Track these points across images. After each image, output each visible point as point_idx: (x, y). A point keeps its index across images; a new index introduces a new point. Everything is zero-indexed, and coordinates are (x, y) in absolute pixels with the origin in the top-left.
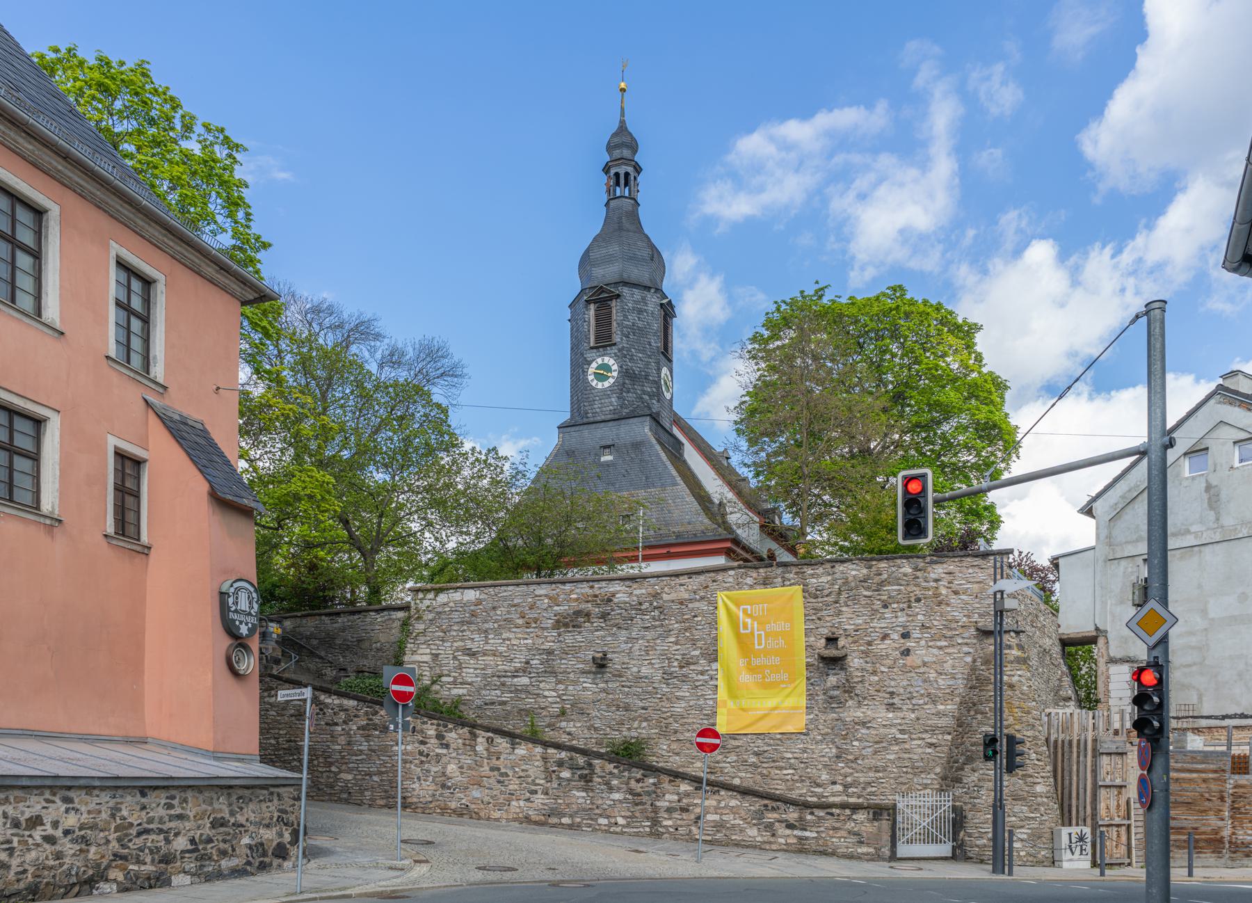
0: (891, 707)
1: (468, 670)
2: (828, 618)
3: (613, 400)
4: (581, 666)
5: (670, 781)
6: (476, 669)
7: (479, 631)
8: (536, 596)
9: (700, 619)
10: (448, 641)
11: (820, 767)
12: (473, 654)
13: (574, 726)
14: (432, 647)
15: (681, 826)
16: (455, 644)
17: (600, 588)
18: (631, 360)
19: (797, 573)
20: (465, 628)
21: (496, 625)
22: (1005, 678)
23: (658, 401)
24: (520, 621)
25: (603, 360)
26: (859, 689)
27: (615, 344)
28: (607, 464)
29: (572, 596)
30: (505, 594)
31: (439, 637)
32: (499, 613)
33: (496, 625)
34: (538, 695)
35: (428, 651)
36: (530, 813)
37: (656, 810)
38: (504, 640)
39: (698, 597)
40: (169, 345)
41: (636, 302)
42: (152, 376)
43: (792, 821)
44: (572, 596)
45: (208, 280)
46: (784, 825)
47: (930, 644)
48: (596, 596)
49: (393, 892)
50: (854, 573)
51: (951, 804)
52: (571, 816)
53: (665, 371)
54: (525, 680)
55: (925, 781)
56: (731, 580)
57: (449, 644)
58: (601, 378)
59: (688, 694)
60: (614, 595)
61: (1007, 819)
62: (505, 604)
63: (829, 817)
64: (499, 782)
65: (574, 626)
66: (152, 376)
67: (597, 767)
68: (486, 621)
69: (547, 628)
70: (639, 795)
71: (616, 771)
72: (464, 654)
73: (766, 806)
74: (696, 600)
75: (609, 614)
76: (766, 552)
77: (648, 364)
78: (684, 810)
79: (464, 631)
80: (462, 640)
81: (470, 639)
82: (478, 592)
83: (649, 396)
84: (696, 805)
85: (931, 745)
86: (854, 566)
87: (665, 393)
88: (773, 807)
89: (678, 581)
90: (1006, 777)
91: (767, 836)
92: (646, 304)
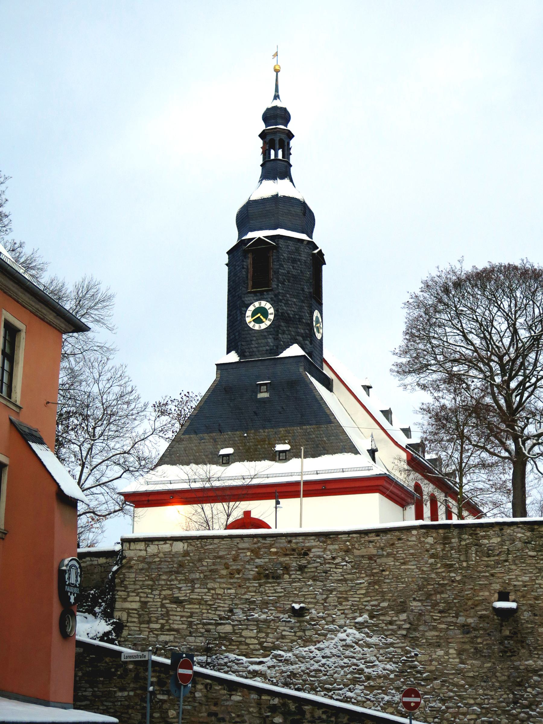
1: (175, 618)
2: (499, 575)
3: (269, 340)
6: (182, 616)
7: (186, 580)
9: (387, 573)
10: (156, 589)
11: (500, 712)
12: (177, 601)
14: (142, 595)
16: (164, 593)
17: (297, 543)
18: (286, 304)
19: (471, 535)
20: (173, 577)
21: (202, 575)
23: (311, 343)
24: (224, 572)
25: (260, 304)
26: (530, 640)
27: (271, 290)
28: (263, 400)
29: (272, 550)
30: (211, 547)
31: (148, 585)
32: (205, 564)
33: (202, 575)
34: (240, 642)
35: (137, 599)
38: (209, 589)
39: (385, 553)
40: (25, 375)
41: (290, 253)
42: (13, 400)
44: (272, 550)
45: (47, 323)
48: (294, 550)
50: (519, 535)
53: (316, 313)
54: (228, 628)
57: (157, 592)
60: (309, 550)
62: (211, 556)
65: (273, 578)
66: (13, 400)
68: (191, 572)
69: (249, 579)
71: (324, 717)
72: (172, 602)
74: (383, 556)
75: (305, 567)
77: (301, 308)
79: (172, 580)
80: (170, 589)
82: (186, 545)
83: (303, 337)
86: (519, 530)
87: (317, 334)
89: (367, 538)
92: (300, 254)
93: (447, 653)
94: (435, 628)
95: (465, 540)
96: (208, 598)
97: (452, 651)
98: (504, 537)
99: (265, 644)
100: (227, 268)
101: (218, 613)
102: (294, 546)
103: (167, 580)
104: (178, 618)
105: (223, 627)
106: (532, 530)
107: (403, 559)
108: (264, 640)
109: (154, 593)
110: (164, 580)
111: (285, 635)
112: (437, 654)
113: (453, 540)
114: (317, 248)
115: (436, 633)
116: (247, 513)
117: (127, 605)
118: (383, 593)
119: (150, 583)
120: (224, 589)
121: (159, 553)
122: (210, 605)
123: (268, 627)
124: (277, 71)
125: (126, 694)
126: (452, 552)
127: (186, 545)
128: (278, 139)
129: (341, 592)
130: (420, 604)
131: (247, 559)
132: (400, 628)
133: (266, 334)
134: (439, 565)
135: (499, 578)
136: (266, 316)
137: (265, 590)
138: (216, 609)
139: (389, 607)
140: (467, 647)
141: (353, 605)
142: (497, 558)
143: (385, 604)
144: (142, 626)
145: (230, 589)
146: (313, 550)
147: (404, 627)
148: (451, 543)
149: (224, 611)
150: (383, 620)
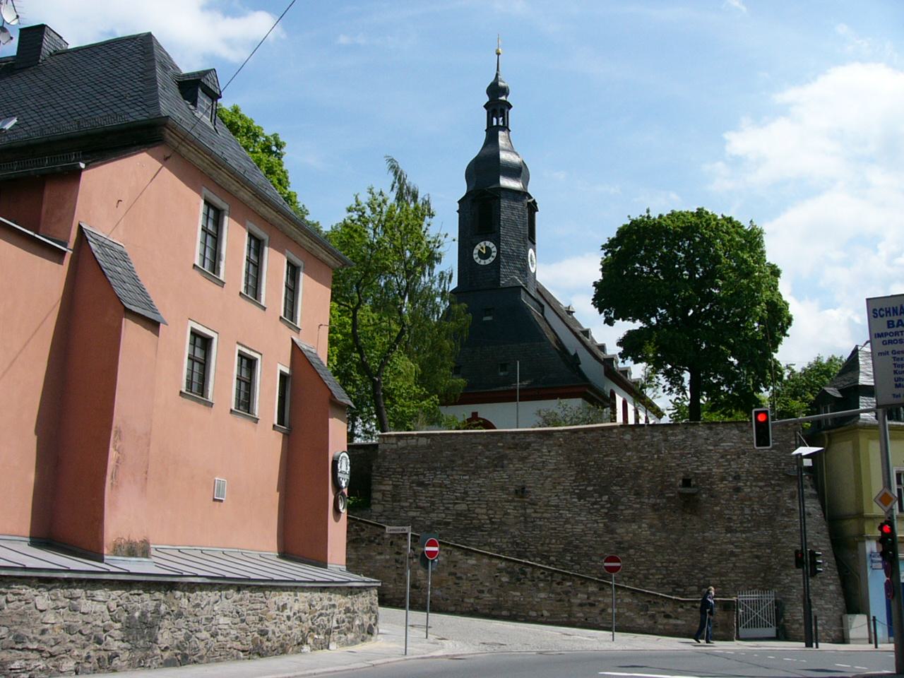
0: (729, 530)
1: (421, 498)
4: (504, 496)
5: (581, 584)
8: (473, 444)
10: (405, 475)
13: (501, 542)
14: (394, 479)
15: (590, 617)
22: (806, 509)
29: (499, 444)
35: (391, 482)
36: (479, 607)
37: (571, 605)
38: (448, 476)
43: (668, 613)
44: (499, 444)
46: (663, 614)
47: (754, 484)
48: (517, 444)
49: (454, 655)
51: (774, 599)
52: (508, 610)
53: (531, 251)
55: (754, 583)
56: (614, 436)
58: (484, 256)
59: (585, 519)
61: (813, 610)
63: (693, 609)
64: (456, 584)
67: (528, 573)
70: (559, 594)
73: (649, 602)
76: (609, 391)
78: (592, 605)
81: (423, 474)
83: (519, 271)
84: (599, 601)
85: (757, 557)
87: (531, 268)
88: (654, 603)
90: (810, 580)
91: (651, 623)
93: (640, 527)
94: (631, 507)
95: (656, 436)
96: (446, 482)
97: (644, 525)
98: (689, 435)
99: (493, 520)
100: (458, 214)
101: (455, 494)
102: (517, 441)
103: (414, 468)
104: (423, 498)
105: (459, 505)
106: (711, 429)
107: (606, 452)
108: (493, 516)
109: (404, 478)
110: (411, 468)
111: (509, 513)
112: (633, 527)
113: (647, 437)
114: (532, 198)
115: (631, 511)
116: (475, 415)
117: (383, 488)
118: (589, 480)
119: (400, 470)
120: (460, 475)
121: (408, 446)
122: (449, 488)
123: (496, 506)
124: (498, 54)
125: (383, 557)
126: (796, 466)
127: (429, 440)
128: (499, 108)
129: (555, 479)
130: (619, 488)
131: (479, 451)
132: (603, 507)
133: (489, 268)
134: (635, 457)
135: (683, 467)
136: (480, 253)
137: (494, 477)
138: (454, 492)
139: (595, 491)
140: (655, 522)
141: (564, 489)
142: (682, 451)
143: (590, 488)
144: (394, 504)
145: (465, 475)
146: (532, 445)
147: (606, 506)
148: (644, 439)
149: (461, 493)
150: (589, 501)
